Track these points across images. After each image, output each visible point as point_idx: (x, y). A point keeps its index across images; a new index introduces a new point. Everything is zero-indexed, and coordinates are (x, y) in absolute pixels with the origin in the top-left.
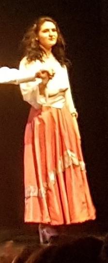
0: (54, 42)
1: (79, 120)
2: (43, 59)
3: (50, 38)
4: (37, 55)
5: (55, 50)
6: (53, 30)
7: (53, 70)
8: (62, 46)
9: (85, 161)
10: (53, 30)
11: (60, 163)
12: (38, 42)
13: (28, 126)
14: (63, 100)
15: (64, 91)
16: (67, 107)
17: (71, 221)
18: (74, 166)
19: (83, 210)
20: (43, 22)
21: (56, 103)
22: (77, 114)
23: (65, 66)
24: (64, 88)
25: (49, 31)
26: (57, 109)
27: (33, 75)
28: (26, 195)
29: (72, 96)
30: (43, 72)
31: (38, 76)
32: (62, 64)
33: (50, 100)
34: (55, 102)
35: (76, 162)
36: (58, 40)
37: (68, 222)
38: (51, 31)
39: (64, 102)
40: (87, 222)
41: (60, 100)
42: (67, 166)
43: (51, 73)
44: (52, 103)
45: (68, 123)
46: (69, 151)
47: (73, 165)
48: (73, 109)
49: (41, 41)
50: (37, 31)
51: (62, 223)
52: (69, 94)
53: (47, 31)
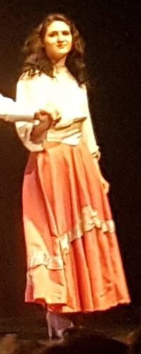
0: (65, 50)
1: (100, 163)
2: (55, 74)
3: (58, 44)
4: (46, 64)
5: (71, 63)
6: (65, 33)
7: (58, 114)
8: (79, 55)
9: (115, 218)
10: (65, 33)
11: (78, 227)
12: (44, 50)
13: (28, 180)
14: (79, 134)
15: (82, 120)
16: (84, 144)
17: (94, 303)
18: (98, 229)
19: (109, 288)
20: (50, 22)
21: (68, 139)
22: (99, 154)
23: (84, 86)
24: (80, 116)
25: (59, 34)
26: (72, 146)
27: (32, 115)
28: (31, 262)
29: (94, 129)
30: (43, 113)
31: (36, 117)
32: (80, 84)
33: (61, 134)
34: (67, 137)
35: (98, 223)
36: (73, 46)
37: (91, 309)
38: (60, 34)
39: (78, 137)
40: (112, 310)
41: (73, 135)
42: (88, 228)
43: (55, 117)
44: (64, 138)
45: (86, 166)
46: (89, 207)
47: (96, 227)
48: (93, 147)
49: (48, 48)
50: (42, 34)
51: (76, 309)
52: (88, 126)
53: (54, 34)
